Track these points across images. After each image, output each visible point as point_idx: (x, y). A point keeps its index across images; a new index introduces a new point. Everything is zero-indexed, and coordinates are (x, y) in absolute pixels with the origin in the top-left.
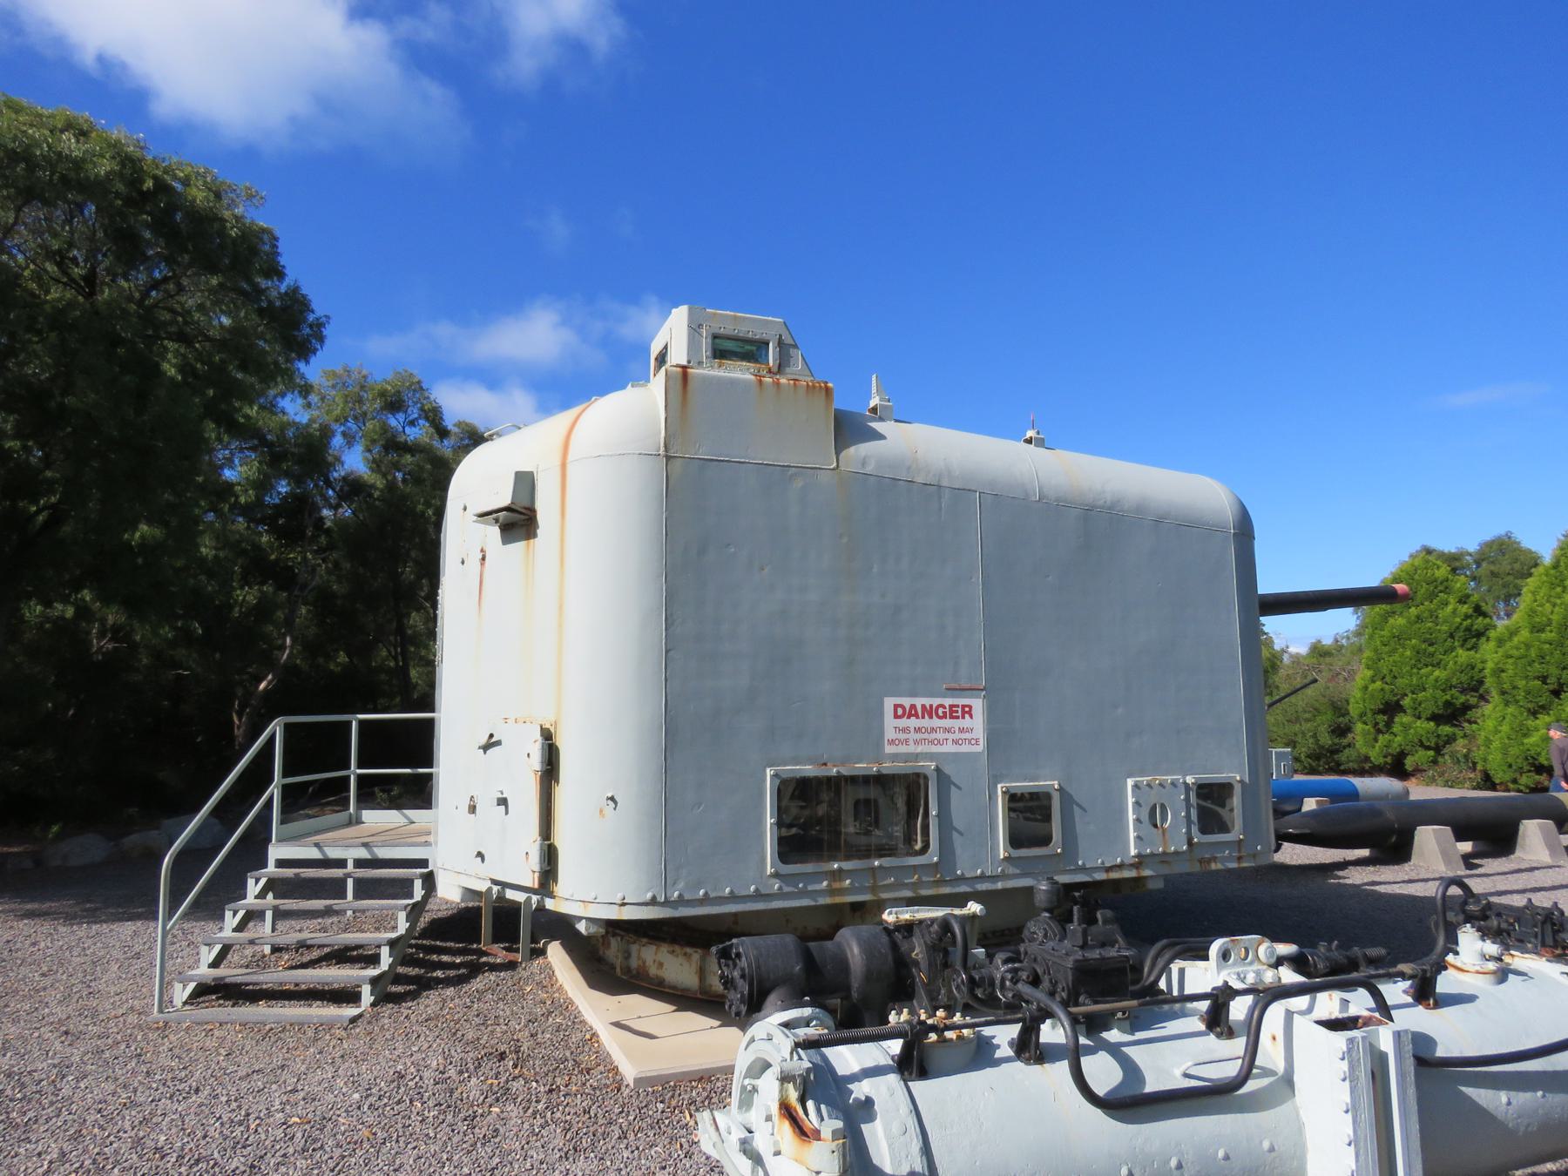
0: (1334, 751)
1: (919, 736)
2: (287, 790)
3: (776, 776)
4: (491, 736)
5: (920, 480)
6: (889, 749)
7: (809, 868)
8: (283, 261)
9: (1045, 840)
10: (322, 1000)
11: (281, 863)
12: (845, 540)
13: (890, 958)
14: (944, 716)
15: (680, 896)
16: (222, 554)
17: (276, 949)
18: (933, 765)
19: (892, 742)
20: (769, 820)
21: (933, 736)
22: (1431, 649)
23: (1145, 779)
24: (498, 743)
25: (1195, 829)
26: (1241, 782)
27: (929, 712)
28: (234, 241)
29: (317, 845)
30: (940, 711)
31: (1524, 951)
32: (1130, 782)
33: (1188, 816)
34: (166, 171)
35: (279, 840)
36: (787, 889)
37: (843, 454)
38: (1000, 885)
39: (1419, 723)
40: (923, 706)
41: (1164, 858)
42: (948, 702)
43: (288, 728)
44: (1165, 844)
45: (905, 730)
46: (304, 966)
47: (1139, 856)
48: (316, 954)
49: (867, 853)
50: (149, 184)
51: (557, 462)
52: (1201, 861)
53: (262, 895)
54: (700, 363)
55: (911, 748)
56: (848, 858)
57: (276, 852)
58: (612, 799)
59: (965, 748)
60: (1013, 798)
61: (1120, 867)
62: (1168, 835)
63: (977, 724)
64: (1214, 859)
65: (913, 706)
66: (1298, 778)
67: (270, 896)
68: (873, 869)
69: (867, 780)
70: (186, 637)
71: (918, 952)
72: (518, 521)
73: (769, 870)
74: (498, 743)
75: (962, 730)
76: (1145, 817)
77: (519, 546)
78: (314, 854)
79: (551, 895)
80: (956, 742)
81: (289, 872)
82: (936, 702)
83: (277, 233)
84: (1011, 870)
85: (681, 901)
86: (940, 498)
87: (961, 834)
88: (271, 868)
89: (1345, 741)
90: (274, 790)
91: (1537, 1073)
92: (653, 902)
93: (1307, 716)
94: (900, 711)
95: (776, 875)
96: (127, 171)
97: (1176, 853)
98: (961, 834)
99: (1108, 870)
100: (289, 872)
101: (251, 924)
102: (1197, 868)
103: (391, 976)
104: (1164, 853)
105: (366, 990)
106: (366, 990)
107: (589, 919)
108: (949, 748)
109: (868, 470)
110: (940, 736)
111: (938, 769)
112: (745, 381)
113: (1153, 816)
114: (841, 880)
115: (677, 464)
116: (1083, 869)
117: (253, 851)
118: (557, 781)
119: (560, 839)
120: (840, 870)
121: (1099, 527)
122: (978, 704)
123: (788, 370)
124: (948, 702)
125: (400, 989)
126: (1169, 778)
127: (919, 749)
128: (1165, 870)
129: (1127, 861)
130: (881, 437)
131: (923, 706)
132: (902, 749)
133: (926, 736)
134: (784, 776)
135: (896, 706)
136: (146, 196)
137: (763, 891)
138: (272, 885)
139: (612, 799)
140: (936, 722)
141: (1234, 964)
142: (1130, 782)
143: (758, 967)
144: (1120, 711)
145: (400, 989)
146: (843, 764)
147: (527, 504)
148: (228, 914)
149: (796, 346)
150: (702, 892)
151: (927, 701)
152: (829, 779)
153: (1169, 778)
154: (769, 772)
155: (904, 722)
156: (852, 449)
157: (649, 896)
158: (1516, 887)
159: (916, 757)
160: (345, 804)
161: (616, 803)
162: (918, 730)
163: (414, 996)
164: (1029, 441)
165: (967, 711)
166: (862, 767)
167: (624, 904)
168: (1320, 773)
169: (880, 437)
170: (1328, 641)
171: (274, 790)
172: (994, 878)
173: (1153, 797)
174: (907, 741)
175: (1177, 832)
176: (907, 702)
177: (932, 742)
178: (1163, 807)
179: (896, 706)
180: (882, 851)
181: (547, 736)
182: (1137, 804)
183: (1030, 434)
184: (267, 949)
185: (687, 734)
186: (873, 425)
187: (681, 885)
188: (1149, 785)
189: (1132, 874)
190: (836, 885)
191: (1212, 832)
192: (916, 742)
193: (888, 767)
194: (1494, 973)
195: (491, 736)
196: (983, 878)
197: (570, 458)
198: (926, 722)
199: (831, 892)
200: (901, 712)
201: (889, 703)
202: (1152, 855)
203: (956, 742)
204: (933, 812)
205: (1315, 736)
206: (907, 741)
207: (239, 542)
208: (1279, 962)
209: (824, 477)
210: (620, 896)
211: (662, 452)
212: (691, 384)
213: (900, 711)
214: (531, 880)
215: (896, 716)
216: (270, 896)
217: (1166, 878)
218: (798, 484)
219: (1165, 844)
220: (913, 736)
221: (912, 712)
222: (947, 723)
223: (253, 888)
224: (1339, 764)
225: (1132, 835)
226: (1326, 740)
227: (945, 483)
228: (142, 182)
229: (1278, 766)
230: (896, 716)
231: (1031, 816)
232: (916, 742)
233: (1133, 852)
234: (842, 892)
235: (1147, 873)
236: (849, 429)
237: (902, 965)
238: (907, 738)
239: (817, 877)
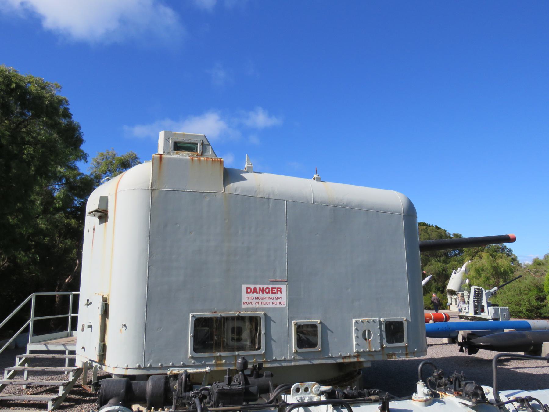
0: (538, 308)
1: (257, 301)
2: (36, 323)
3: (193, 316)
4: (88, 300)
5: (260, 196)
6: (244, 306)
7: (207, 355)
8: (71, 111)
9: (314, 345)
10: (34, 407)
11: (32, 352)
12: (227, 221)
13: (163, 388)
14: (269, 292)
15: (151, 365)
16: (49, 227)
17: (28, 387)
18: (263, 313)
19: (245, 303)
20: (190, 335)
21: (264, 301)
23: (361, 319)
24: (91, 303)
25: (384, 341)
26: (407, 320)
27: (262, 291)
28: (47, 106)
29: (45, 345)
30: (267, 290)
31: (450, 393)
32: (354, 320)
33: (381, 335)
34: (20, 80)
35: (32, 343)
36: (197, 364)
37: (227, 187)
38: (293, 364)
40: (260, 289)
41: (370, 353)
42: (270, 286)
43: (37, 297)
44: (370, 347)
45: (251, 298)
46: (36, 394)
47: (357, 352)
48: (43, 389)
49: (233, 349)
50: (14, 85)
51: (115, 192)
52: (388, 355)
53: (23, 364)
54: (168, 153)
55: (254, 306)
56: (225, 351)
57: (30, 347)
58: (125, 325)
59: (278, 306)
60: (299, 328)
61: (349, 357)
62: (371, 344)
63: (284, 296)
64: (395, 354)
65: (255, 288)
66: (512, 320)
67: (26, 365)
68: (235, 356)
69: (233, 319)
70: (34, 261)
71: (176, 386)
72: (103, 215)
73: (189, 356)
74: (91, 303)
75: (276, 298)
76: (360, 334)
77: (103, 224)
78: (43, 348)
79: (104, 364)
80: (274, 303)
81: (32, 355)
82: (265, 286)
83: (68, 99)
84: (298, 357)
85: (151, 368)
86: (269, 203)
87: (275, 341)
88: (28, 354)
89: (543, 304)
90: (30, 322)
92: (139, 368)
93: (526, 292)
94: (249, 290)
95: (192, 357)
96: (6, 81)
97: (375, 351)
98: (275, 341)
99: (344, 358)
100: (32, 355)
101: (16, 377)
102: (386, 358)
103: (64, 399)
104: (369, 351)
105: (50, 403)
106: (50, 403)
107: (116, 375)
108: (271, 306)
109: (238, 193)
110: (267, 300)
111: (265, 314)
112: (187, 160)
113: (365, 335)
114: (221, 360)
115: (156, 193)
116: (331, 357)
117: (19, 348)
118: (108, 318)
119: (109, 342)
120: (220, 356)
121: (340, 215)
122: (284, 288)
123: (205, 154)
124: (270, 286)
125: (67, 404)
126: (372, 319)
127: (258, 306)
128: (371, 359)
129: (352, 355)
130: (245, 179)
131: (260, 289)
132: (250, 306)
133: (261, 301)
134: (197, 317)
135: (247, 288)
136: (13, 90)
137: (187, 364)
138: (27, 360)
139: (125, 325)
140: (265, 295)
141: (301, 394)
142: (354, 320)
143: (106, 390)
144: (349, 290)
145: (67, 404)
146: (223, 312)
147: (105, 209)
148: (6, 372)
149: (209, 145)
150: (160, 364)
151: (261, 286)
152: (217, 319)
153: (372, 319)
154: (191, 315)
155: (251, 295)
156: (231, 185)
157: (137, 365)
158: (540, 368)
159: (256, 309)
160: (67, 330)
161: (126, 327)
162: (257, 298)
163: (71, 407)
164: (314, 179)
165: (279, 290)
166: (232, 314)
167: (127, 369)
168: (520, 317)
169: (245, 179)
170: (541, 258)
171: (30, 322)
172: (290, 361)
173: (365, 327)
174: (252, 303)
175: (376, 342)
176: (252, 287)
177: (263, 303)
178: (369, 331)
179: (247, 288)
180: (239, 349)
181: (105, 301)
182: (357, 330)
183: (315, 176)
184: (24, 387)
185: (156, 299)
186: (243, 175)
187: (151, 361)
188: (362, 322)
189: (355, 360)
190: (219, 362)
191: (393, 343)
192: (256, 303)
193: (243, 313)
194: (425, 401)
195: (88, 300)
196: (285, 360)
197: (118, 191)
198: (261, 295)
199: (217, 365)
200: (249, 291)
201: (244, 287)
202: (364, 352)
203: (274, 303)
204: (263, 332)
205: (529, 301)
206: (252, 303)
207: (56, 222)
208: (322, 393)
209: (218, 196)
210: (126, 365)
211: (150, 188)
212: (163, 161)
213: (249, 290)
214: (96, 358)
215: (247, 292)
216: (26, 365)
217: (372, 362)
218: (207, 199)
219: (370, 347)
220: (255, 301)
221: (255, 291)
222: (270, 295)
223: (18, 362)
224: (541, 314)
225: (354, 343)
226: (535, 303)
227: (271, 197)
228: (11, 84)
229: (502, 315)
230: (247, 292)
231: (306, 336)
232: (256, 303)
233: (355, 350)
234: (221, 365)
235: (362, 359)
236: (230, 175)
237: (168, 390)
238: (250, 302)
239: (211, 358)
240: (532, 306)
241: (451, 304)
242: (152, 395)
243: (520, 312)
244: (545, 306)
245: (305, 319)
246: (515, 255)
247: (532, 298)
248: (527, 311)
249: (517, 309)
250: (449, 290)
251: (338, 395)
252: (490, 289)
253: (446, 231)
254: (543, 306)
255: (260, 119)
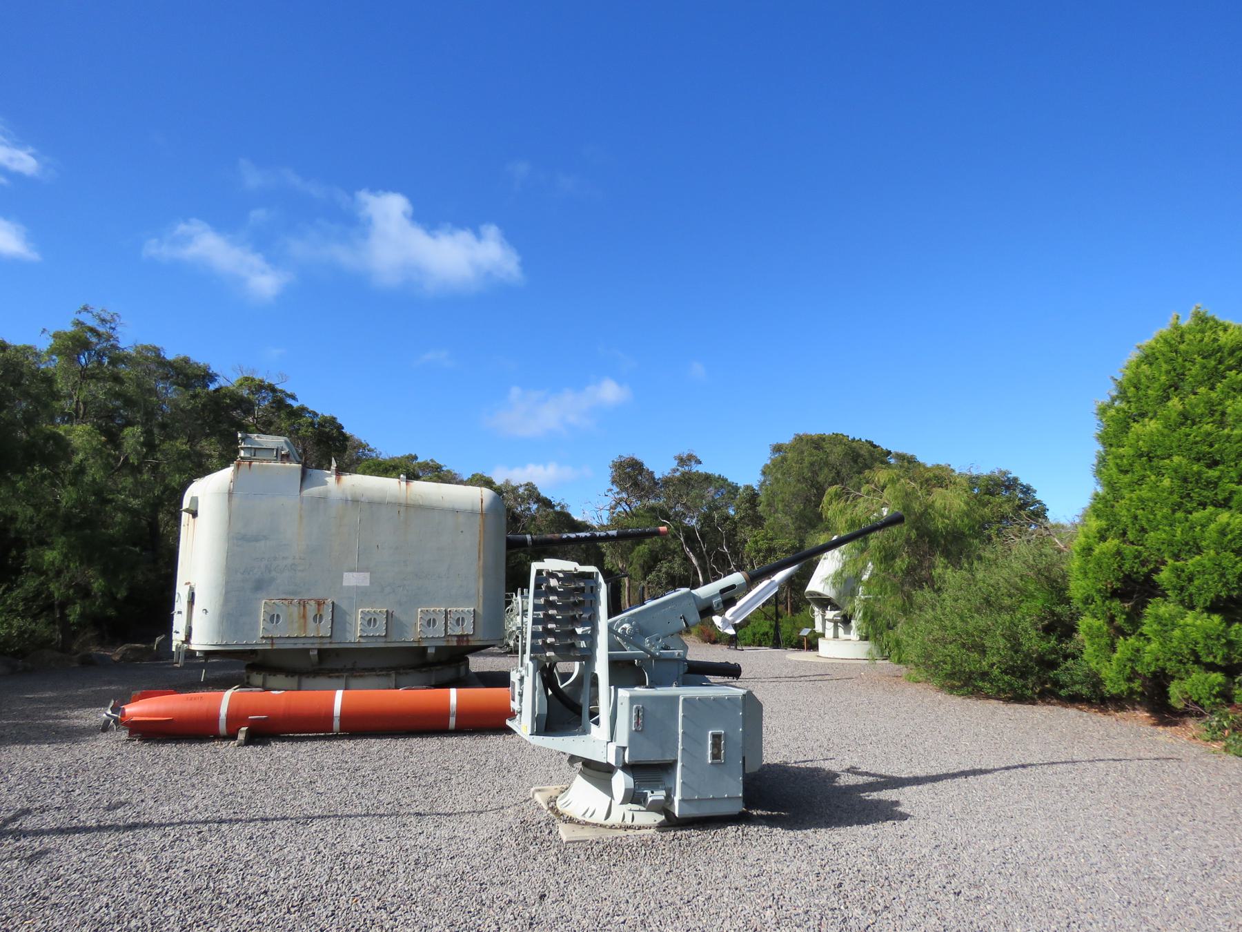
0: (1048, 664)
22: (1213, 473)
39: (1190, 617)
89: (1070, 647)
91: (590, 564)
224: (1056, 683)
226: (1034, 643)
240: (1028, 655)
241: (823, 635)
242: (344, 715)
243: (984, 675)
244: (1074, 657)
245: (717, 700)
246: (1039, 502)
247: (1027, 623)
248: (1005, 672)
249: (975, 662)
250: (812, 593)
251: (81, 470)
252: (560, 532)
253: (766, 466)
254: (1066, 657)
255: (610, 392)
